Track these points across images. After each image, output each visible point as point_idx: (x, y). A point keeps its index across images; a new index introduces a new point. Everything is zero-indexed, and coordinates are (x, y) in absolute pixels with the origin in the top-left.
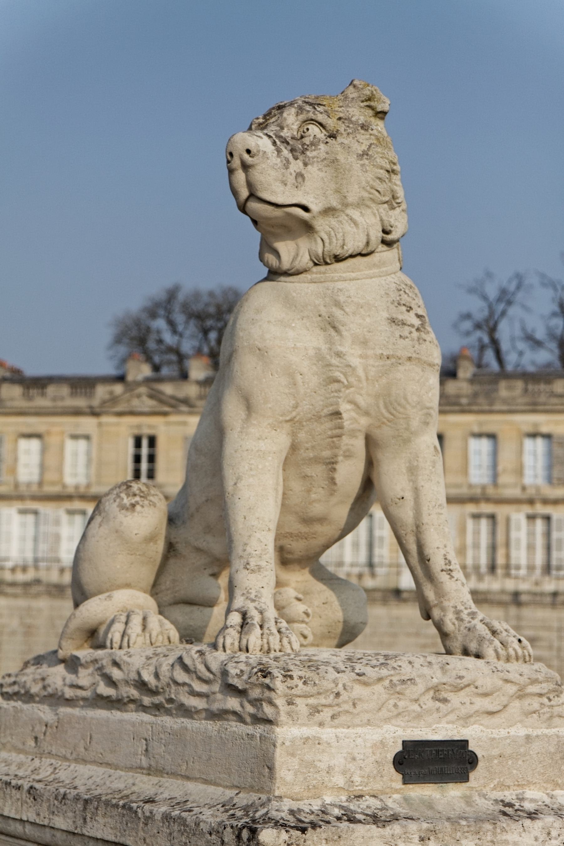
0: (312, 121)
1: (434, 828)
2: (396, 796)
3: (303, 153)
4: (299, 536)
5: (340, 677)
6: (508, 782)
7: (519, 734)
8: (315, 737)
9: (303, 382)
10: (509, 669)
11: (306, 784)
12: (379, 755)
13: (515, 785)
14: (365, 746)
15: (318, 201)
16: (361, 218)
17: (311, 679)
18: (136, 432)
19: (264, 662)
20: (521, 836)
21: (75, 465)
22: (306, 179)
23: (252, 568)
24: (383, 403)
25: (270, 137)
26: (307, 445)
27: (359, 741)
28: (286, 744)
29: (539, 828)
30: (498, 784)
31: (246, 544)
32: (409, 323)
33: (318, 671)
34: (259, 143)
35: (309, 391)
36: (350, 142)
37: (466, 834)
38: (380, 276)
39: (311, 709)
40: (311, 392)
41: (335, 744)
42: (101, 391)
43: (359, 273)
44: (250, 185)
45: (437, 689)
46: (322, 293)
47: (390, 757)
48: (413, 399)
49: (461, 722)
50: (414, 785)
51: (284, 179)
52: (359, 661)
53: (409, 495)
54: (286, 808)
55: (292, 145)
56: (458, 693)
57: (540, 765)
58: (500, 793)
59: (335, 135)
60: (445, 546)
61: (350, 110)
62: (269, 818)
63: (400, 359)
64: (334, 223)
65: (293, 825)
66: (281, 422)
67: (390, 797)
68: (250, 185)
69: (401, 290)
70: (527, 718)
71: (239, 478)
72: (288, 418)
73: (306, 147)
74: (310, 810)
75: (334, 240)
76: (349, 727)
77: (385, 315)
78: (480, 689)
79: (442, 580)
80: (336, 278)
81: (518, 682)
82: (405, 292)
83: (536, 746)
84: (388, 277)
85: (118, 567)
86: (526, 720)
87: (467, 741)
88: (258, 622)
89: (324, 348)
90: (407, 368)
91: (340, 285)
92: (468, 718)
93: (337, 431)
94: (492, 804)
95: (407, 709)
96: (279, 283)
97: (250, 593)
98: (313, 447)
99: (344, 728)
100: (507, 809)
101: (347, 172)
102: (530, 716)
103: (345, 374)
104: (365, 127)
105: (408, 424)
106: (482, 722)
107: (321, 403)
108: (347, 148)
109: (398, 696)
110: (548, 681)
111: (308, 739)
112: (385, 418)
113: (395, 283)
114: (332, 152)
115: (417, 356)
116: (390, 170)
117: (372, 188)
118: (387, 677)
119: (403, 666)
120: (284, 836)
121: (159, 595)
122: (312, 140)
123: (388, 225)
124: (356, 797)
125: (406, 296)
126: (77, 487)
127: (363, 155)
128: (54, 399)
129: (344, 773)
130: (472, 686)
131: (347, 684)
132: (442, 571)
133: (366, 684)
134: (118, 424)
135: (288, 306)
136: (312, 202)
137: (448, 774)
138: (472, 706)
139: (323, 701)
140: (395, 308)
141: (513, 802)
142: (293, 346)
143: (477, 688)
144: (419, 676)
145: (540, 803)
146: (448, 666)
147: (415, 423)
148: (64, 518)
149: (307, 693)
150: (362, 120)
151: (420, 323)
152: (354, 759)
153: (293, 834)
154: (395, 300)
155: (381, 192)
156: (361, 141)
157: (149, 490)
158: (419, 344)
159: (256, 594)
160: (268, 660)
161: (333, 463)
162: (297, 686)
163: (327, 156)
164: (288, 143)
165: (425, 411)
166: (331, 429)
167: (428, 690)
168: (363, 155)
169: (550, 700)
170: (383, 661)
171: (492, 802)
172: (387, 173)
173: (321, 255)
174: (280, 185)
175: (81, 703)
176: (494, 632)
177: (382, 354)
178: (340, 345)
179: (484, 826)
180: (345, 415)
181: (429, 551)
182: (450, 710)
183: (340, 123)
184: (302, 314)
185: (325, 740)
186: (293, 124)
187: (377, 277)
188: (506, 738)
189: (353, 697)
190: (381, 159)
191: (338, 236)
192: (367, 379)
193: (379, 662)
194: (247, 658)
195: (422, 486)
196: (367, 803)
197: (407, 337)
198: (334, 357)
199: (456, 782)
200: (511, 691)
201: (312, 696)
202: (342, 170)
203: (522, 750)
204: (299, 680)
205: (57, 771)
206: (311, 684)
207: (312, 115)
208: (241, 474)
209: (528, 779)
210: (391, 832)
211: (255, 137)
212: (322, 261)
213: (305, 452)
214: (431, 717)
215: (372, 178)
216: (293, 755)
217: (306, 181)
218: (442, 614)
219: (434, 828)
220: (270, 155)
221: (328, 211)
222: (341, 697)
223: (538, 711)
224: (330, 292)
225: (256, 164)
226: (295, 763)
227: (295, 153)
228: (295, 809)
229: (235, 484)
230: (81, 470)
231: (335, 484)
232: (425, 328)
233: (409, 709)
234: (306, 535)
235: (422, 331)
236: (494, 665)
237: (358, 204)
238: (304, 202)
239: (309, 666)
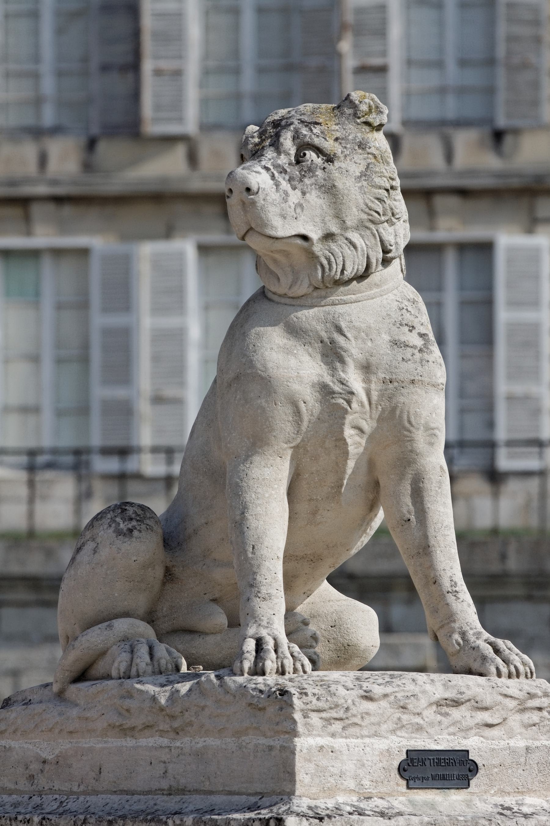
2: (401, 798)
3: (301, 181)
6: (508, 789)
7: (518, 745)
9: (307, 410)
10: (510, 685)
19: (280, 683)
25: (267, 169)
28: (304, 752)
32: (411, 344)
33: (329, 689)
41: (345, 752)
43: (360, 295)
46: (323, 317)
47: (396, 764)
51: (284, 213)
52: (367, 680)
54: (305, 805)
57: (540, 774)
58: (500, 799)
59: (333, 158)
62: (291, 812)
65: (311, 816)
69: (403, 308)
74: (326, 807)
75: (334, 266)
76: (358, 738)
83: (535, 757)
85: (116, 595)
87: (468, 751)
88: (272, 647)
92: (468, 730)
94: (492, 807)
99: (353, 738)
100: (505, 812)
102: (530, 728)
106: (482, 734)
109: (402, 710)
118: (391, 693)
119: (406, 684)
121: (155, 623)
124: (365, 798)
125: (408, 314)
136: (311, 231)
140: (397, 329)
141: (512, 806)
145: (538, 808)
151: (423, 342)
152: (363, 765)
153: (313, 821)
154: (397, 320)
157: (145, 513)
160: (284, 681)
162: (311, 702)
164: (285, 172)
168: (361, 176)
170: (389, 680)
193: (385, 681)
194: (264, 680)
196: (376, 803)
197: (409, 360)
200: (510, 705)
201: (325, 710)
204: (313, 697)
205: (65, 804)
211: (254, 173)
214: (433, 729)
216: (310, 761)
222: (351, 711)
224: (331, 317)
226: (311, 767)
227: (293, 183)
228: (313, 806)
232: (428, 348)
234: (312, 558)
236: (495, 682)
238: (303, 232)
239: (321, 685)
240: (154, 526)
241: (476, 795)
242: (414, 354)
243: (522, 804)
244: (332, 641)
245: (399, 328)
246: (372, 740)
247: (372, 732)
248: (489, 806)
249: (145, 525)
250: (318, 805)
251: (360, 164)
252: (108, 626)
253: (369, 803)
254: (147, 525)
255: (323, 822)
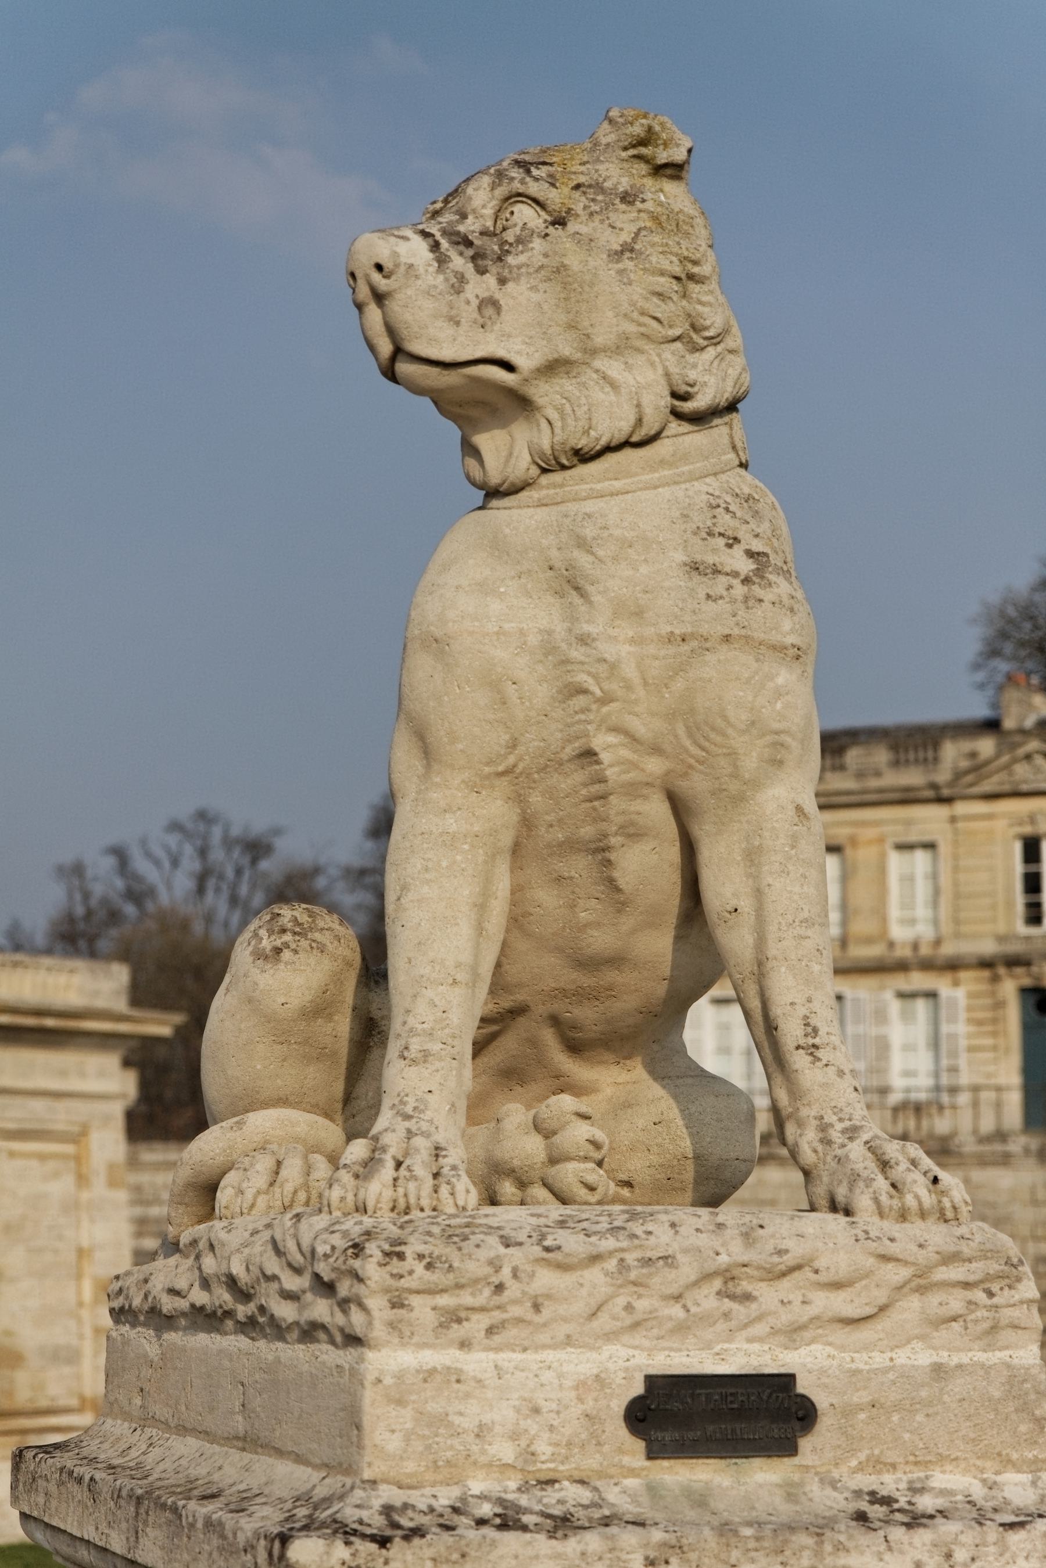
0: (519, 196)
1: (679, 1541)
2: (631, 1482)
4: (581, 995)
5: (506, 1255)
6: (891, 1456)
7: (916, 1363)
8: (449, 1368)
10: (897, 1235)
11: (431, 1457)
12: (591, 1403)
13: (907, 1463)
14: (561, 1385)
15: (533, 349)
16: (626, 374)
17: (444, 1259)
18: (1028, 830)
20: (881, 1560)
21: (908, 903)
22: (504, 308)
23: (412, 1056)
24: (684, 729)
26: (548, 818)
27: (547, 1376)
29: (924, 1545)
30: (868, 1460)
31: (408, 1011)
32: (728, 569)
34: (398, 249)
35: (533, 713)
36: (594, 229)
37: (753, 1554)
38: (676, 483)
39: (442, 1315)
40: (538, 715)
42: (952, 752)
44: (391, 331)
45: (728, 1275)
46: (555, 523)
47: (618, 1406)
48: (740, 717)
49: (782, 1339)
50: (672, 1462)
51: (453, 312)
53: (746, 905)
54: (377, 1503)
55: (478, 247)
56: (777, 1283)
58: (873, 1477)
59: (564, 218)
60: (809, 1000)
61: (601, 167)
63: (706, 640)
64: (570, 388)
66: (488, 777)
67: (616, 1484)
68: (391, 331)
70: (937, 1331)
71: (405, 888)
72: (501, 769)
73: (506, 248)
75: (570, 421)
76: (525, 1350)
77: (680, 557)
78: (824, 1273)
79: (796, 1067)
80: (584, 494)
81: (911, 1259)
82: (727, 510)
83: (958, 1386)
84: (696, 483)
85: (259, 1067)
86: (935, 1334)
87: (791, 1377)
89: (560, 628)
90: (722, 658)
91: (590, 506)
92: (795, 1330)
93: (596, 788)
94: (847, 1499)
95: (654, 1315)
96: (490, 511)
97: (405, 1104)
98: (560, 821)
99: (514, 1351)
101: (587, 289)
102: (944, 1326)
103: (595, 677)
104: (627, 198)
105: (736, 767)
106: (830, 1339)
107: (559, 735)
108: (588, 243)
109: (635, 1289)
110: (987, 1258)
111: (432, 1372)
112: (692, 756)
113: (708, 493)
114: (556, 253)
115: (743, 632)
116: (683, 276)
117: (642, 314)
119: (655, 1232)
120: (341, 1551)
121: (357, 1119)
122: (518, 233)
123: (680, 382)
124: (540, 1482)
125: (728, 517)
126: (916, 946)
127: (622, 252)
128: (860, 775)
129: (514, 1436)
130: (807, 1268)
131: (521, 1267)
132: (798, 1048)
133: (563, 1267)
134: (990, 817)
135: (497, 554)
137: (749, 1439)
138: (807, 1308)
139: (467, 1299)
140: (699, 541)
142: (496, 629)
143: (816, 1272)
144: (685, 1251)
145: (959, 1498)
146: (761, 1231)
147: (750, 764)
148: (895, 1006)
149: (432, 1286)
150: (625, 184)
151: (754, 567)
152: (536, 1410)
154: (701, 526)
155: (662, 319)
156: (618, 225)
157: (314, 921)
158: (748, 608)
159: (416, 1104)
161: (603, 850)
162: (411, 1272)
163: (545, 261)
164: (469, 244)
165: (769, 738)
166: (585, 785)
167: (707, 1277)
168: (622, 252)
169: (991, 1294)
171: (847, 1494)
172: (674, 282)
173: (549, 452)
174: (445, 325)
175: (183, 1322)
176: (884, 1165)
177: (672, 633)
178: (588, 622)
179: (794, 1538)
180: (605, 757)
181: (777, 1011)
182: (754, 1315)
183: (577, 194)
184: (518, 567)
185: (472, 1374)
186: (484, 206)
187: (668, 484)
188: (886, 1371)
189: (532, 1292)
190: (661, 256)
191: (578, 413)
192: (646, 684)
195: (769, 885)
196: (563, 1494)
197: (721, 597)
198: (574, 645)
199: (769, 1457)
202: (576, 285)
203: (924, 1393)
204: (417, 1262)
206: (442, 1269)
207: (519, 185)
208: (409, 880)
209: (940, 1451)
210: (579, 1548)
212: (553, 462)
213: (548, 832)
214: (711, 1329)
215: (641, 294)
216: (400, 1402)
217: (503, 313)
218: (799, 1132)
219: (679, 1541)
220: (422, 270)
221: (553, 367)
222: (507, 1293)
223: (961, 1316)
225: (395, 290)
227: (480, 262)
229: (399, 899)
230: (922, 911)
231: (618, 890)
232: (762, 577)
233: (660, 1314)
235: (754, 583)
237: (618, 347)
238: (501, 353)
240: (329, 944)
241: (813, 1470)
242: (732, 587)
243: (922, 1490)
244: (655, 1149)
245: (704, 539)
246: (560, 1355)
247: (561, 1336)
248: (840, 1497)
249: (308, 942)
250: (411, 1501)
251: (621, 229)
252: (237, 1123)
253: (544, 1493)
254: (314, 941)
255: (388, 1550)
